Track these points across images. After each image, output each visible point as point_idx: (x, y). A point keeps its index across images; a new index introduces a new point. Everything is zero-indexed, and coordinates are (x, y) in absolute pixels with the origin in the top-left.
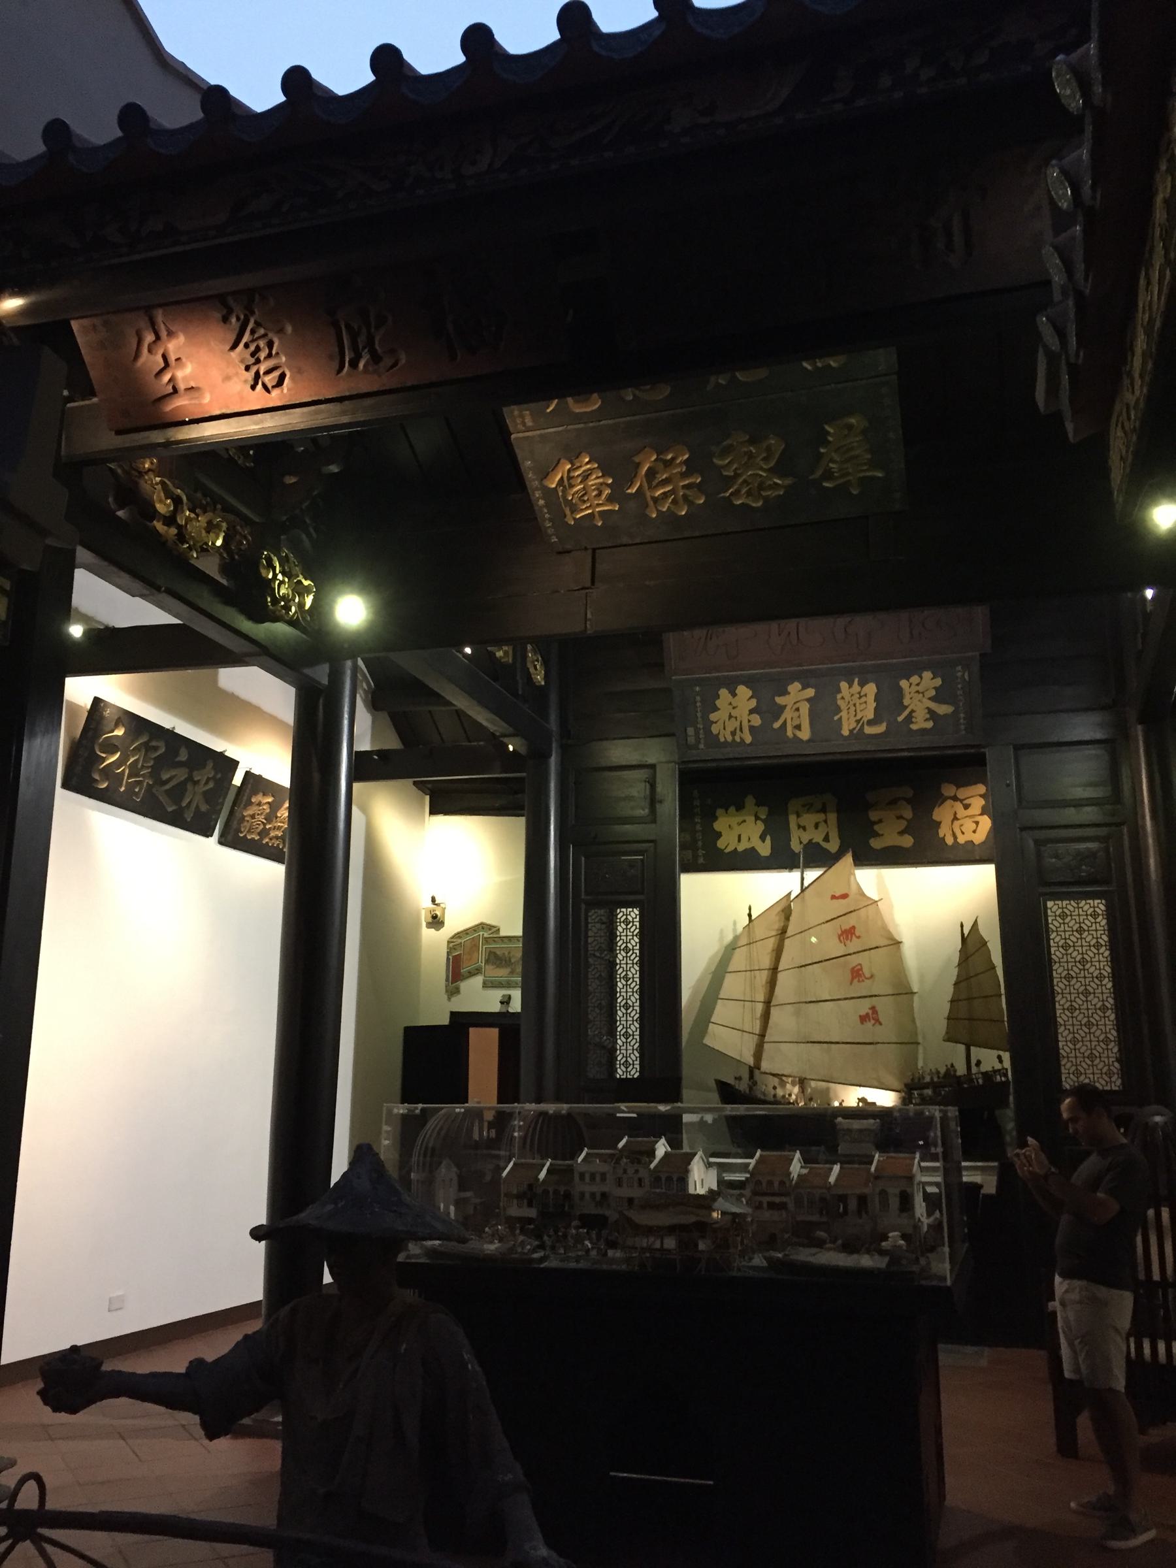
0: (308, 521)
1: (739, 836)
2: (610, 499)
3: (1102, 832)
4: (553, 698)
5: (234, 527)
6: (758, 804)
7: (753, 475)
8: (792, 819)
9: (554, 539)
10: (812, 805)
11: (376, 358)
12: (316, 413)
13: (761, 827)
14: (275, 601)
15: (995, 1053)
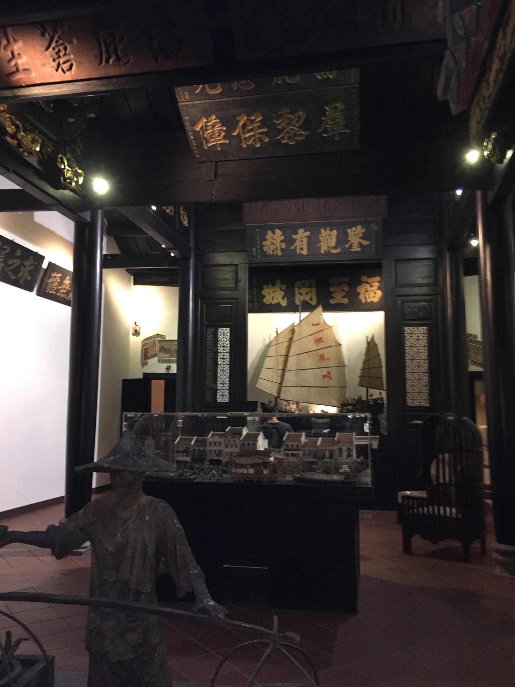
0: (79, 141)
1: (273, 297)
2: (225, 138)
3: (428, 298)
4: (192, 232)
5: (44, 142)
6: (282, 283)
7: (291, 129)
8: (297, 291)
9: (198, 156)
10: (305, 284)
11: (118, 59)
12: (88, 85)
13: (282, 293)
14: (65, 179)
15: (378, 391)
